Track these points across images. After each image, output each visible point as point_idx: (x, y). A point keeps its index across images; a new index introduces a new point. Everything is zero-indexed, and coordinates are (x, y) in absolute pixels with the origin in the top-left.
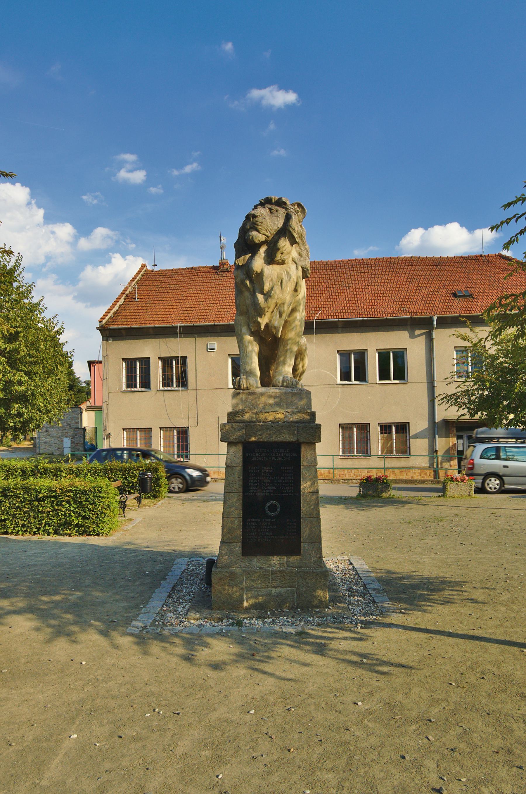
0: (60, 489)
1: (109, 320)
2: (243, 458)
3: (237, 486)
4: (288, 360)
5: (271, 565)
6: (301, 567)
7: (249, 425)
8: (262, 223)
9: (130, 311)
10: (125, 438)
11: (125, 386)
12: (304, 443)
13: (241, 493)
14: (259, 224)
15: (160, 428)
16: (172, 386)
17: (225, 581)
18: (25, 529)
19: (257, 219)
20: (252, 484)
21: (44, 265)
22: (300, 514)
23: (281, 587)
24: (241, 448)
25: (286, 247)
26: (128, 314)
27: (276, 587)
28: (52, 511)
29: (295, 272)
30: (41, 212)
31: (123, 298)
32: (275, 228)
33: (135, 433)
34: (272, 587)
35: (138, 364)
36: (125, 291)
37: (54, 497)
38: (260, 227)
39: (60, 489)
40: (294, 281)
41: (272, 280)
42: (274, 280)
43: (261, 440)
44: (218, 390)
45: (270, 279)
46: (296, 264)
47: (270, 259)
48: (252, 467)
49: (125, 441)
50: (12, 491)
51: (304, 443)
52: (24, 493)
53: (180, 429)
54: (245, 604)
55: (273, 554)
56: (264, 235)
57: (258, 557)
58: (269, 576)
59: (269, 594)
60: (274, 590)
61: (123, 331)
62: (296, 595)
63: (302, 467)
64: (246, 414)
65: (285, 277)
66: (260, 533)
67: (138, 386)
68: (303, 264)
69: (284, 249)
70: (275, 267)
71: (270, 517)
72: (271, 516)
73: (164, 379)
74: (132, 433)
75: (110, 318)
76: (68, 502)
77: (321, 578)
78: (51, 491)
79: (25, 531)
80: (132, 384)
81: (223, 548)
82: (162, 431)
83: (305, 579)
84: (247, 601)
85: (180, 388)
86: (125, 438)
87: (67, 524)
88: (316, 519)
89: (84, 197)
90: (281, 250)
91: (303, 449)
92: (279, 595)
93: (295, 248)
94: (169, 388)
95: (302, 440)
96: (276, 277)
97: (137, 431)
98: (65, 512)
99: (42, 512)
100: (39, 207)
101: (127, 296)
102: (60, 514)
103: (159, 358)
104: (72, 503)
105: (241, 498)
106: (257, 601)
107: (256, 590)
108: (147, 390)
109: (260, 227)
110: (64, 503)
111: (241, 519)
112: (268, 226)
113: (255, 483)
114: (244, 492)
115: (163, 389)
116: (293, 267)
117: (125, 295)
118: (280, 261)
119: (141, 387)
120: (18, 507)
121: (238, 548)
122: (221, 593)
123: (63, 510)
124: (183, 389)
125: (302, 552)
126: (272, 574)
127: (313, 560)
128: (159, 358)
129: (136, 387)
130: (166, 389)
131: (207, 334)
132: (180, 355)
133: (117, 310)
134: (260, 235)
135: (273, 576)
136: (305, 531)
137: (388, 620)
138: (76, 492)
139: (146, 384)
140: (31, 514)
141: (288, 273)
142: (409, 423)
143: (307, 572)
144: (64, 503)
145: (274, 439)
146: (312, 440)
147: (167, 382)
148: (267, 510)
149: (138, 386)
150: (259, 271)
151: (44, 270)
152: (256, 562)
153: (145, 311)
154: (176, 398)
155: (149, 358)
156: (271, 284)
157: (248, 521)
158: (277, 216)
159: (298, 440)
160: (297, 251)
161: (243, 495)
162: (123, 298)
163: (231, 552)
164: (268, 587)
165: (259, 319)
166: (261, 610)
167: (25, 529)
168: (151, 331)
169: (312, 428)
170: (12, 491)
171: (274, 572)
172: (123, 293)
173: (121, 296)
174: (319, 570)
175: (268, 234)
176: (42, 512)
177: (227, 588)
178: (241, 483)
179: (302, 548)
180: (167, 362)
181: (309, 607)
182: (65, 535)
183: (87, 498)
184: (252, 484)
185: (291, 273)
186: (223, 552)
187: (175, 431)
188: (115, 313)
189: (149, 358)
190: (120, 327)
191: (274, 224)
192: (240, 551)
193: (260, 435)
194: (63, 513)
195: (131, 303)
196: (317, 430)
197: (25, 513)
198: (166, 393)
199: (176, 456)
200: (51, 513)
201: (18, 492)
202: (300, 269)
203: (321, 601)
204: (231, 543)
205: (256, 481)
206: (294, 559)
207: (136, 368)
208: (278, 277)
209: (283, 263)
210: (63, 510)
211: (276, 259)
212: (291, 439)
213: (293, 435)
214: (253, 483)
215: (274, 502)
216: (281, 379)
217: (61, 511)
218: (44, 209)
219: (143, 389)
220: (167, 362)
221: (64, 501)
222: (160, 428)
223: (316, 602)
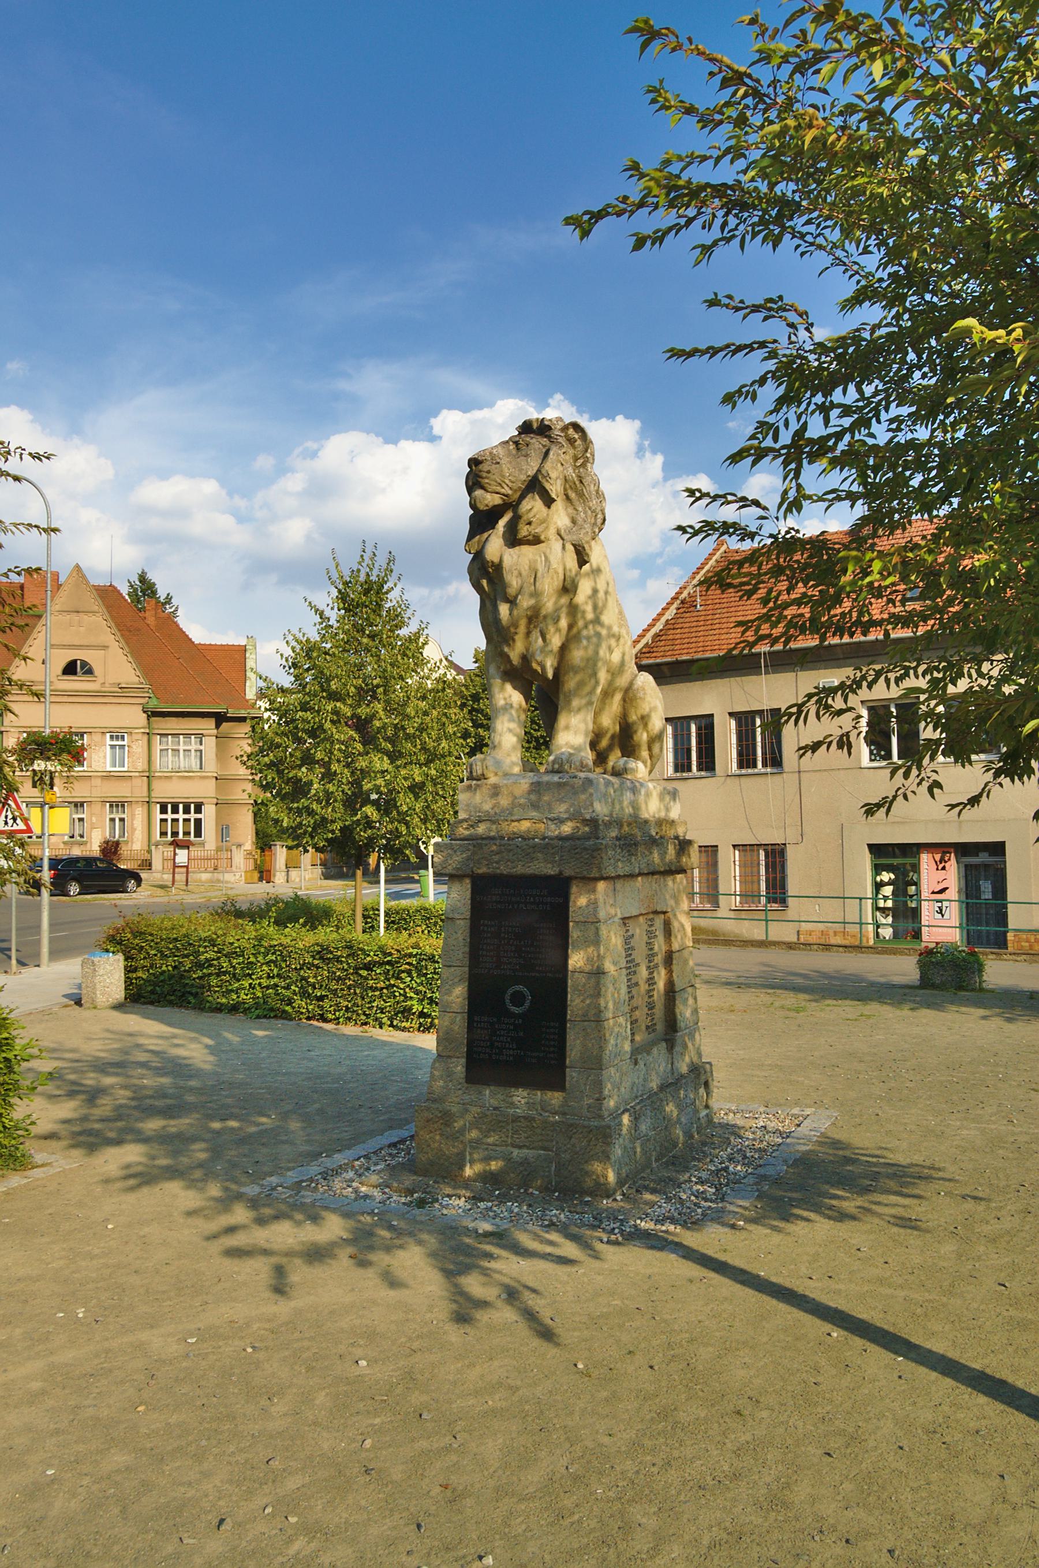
0: (398, 951)
1: (644, 650)
2: (472, 904)
3: (461, 956)
5: (512, 1105)
6: (564, 1114)
8: (488, 472)
9: (683, 631)
10: (737, 863)
11: (735, 765)
13: (467, 969)
14: (484, 475)
15: (734, 846)
16: (755, 766)
17: (436, 1126)
18: (350, 1015)
19: (480, 467)
21: (660, 554)
23: (528, 1148)
24: (469, 886)
25: (535, 510)
26: (677, 637)
27: (520, 1147)
28: (387, 988)
29: (560, 554)
30: (659, 459)
31: (675, 605)
32: (523, 477)
33: (755, 853)
34: (514, 1146)
35: (693, 728)
36: (679, 593)
37: (389, 963)
38: (487, 481)
39: (398, 951)
40: (557, 573)
41: (520, 574)
42: (524, 573)
43: (498, 871)
44: (842, 772)
45: (515, 573)
46: (563, 539)
47: (513, 540)
49: (737, 868)
50: (332, 953)
52: (348, 955)
53: (770, 847)
54: (468, 1172)
55: (517, 1085)
56: (497, 493)
57: (492, 1088)
58: (508, 1124)
59: (508, 1159)
60: (516, 1152)
61: (665, 669)
63: (571, 924)
65: (541, 568)
66: (496, 1044)
67: (694, 768)
68: (575, 537)
69: (531, 515)
70: (525, 549)
71: (513, 1015)
72: (513, 1013)
73: (740, 754)
74: (749, 853)
75: (647, 645)
76: (409, 973)
77: (597, 1139)
78: (386, 954)
79: (349, 1019)
80: (748, 761)
81: (437, 1065)
82: (737, 852)
83: (571, 1138)
84: (471, 1167)
85: (769, 770)
86: (737, 863)
87: (407, 1012)
88: (593, 1024)
89: (731, 425)
90: (525, 518)
91: (574, 889)
92: (525, 1162)
94: (750, 771)
95: (568, 872)
96: (527, 568)
97: (758, 851)
98: (404, 989)
99: (373, 989)
100: (654, 452)
101: (683, 602)
102: (397, 994)
103: (731, 714)
104: (415, 975)
106: (488, 1168)
108: (709, 774)
109: (487, 481)
110: (403, 975)
111: (466, 1015)
112: (503, 476)
114: (471, 967)
115: (738, 772)
116: (556, 545)
117: (679, 602)
118: (530, 538)
119: (699, 769)
120: (340, 978)
121: (459, 1068)
122: (429, 1146)
123: (402, 986)
124: (775, 771)
125: (567, 1085)
127: (587, 1101)
128: (731, 714)
129: (690, 770)
130: (744, 771)
131: (818, 664)
132: (766, 706)
133: (661, 631)
134: (488, 496)
136: (575, 1045)
137: (691, 1239)
138: (422, 957)
139: (708, 762)
140: (358, 991)
141: (546, 558)
143: (572, 1125)
144: (403, 975)
145: (520, 869)
146: (585, 873)
147: (746, 759)
148: (507, 1001)
149: (694, 768)
150: (496, 560)
151: (659, 561)
152: (490, 1096)
153: (709, 627)
154: (765, 789)
155: (712, 715)
156: (520, 582)
158: (526, 456)
159: (561, 873)
160: (568, 515)
161: (470, 970)
162: (675, 605)
163: (449, 1075)
165: (506, 649)
166: (492, 1187)
167: (350, 1014)
168: (665, 669)
169: (585, 849)
170: (332, 953)
171: (516, 1119)
172: (674, 599)
173: (670, 604)
174: (595, 1123)
175: (507, 490)
176: (373, 989)
177: (438, 1137)
178: (467, 949)
179: (567, 1079)
180: (744, 720)
181: (576, 1192)
182: (404, 1029)
183: (435, 968)
185: (552, 558)
186: (436, 1073)
187: (762, 853)
188: (657, 635)
189: (712, 715)
190: (658, 661)
191: (521, 470)
192: (463, 1075)
193: (497, 863)
194: (402, 992)
195: (688, 615)
196: (595, 854)
197: (349, 988)
198: (743, 780)
199: (763, 900)
200: (385, 991)
201: (339, 953)
202: (570, 548)
203: (598, 1184)
204: (449, 1057)
206: (555, 1098)
207: (689, 735)
208: (530, 568)
209: (536, 541)
210: (402, 986)
211: (519, 536)
212: (550, 870)
213: (553, 862)
215: (515, 1010)
217: (398, 987)
218: (662, 453)
219: (703, 773)
220: (744, 720)
221: (403, 972)
222: (734, 846)
223: (589, 1183)
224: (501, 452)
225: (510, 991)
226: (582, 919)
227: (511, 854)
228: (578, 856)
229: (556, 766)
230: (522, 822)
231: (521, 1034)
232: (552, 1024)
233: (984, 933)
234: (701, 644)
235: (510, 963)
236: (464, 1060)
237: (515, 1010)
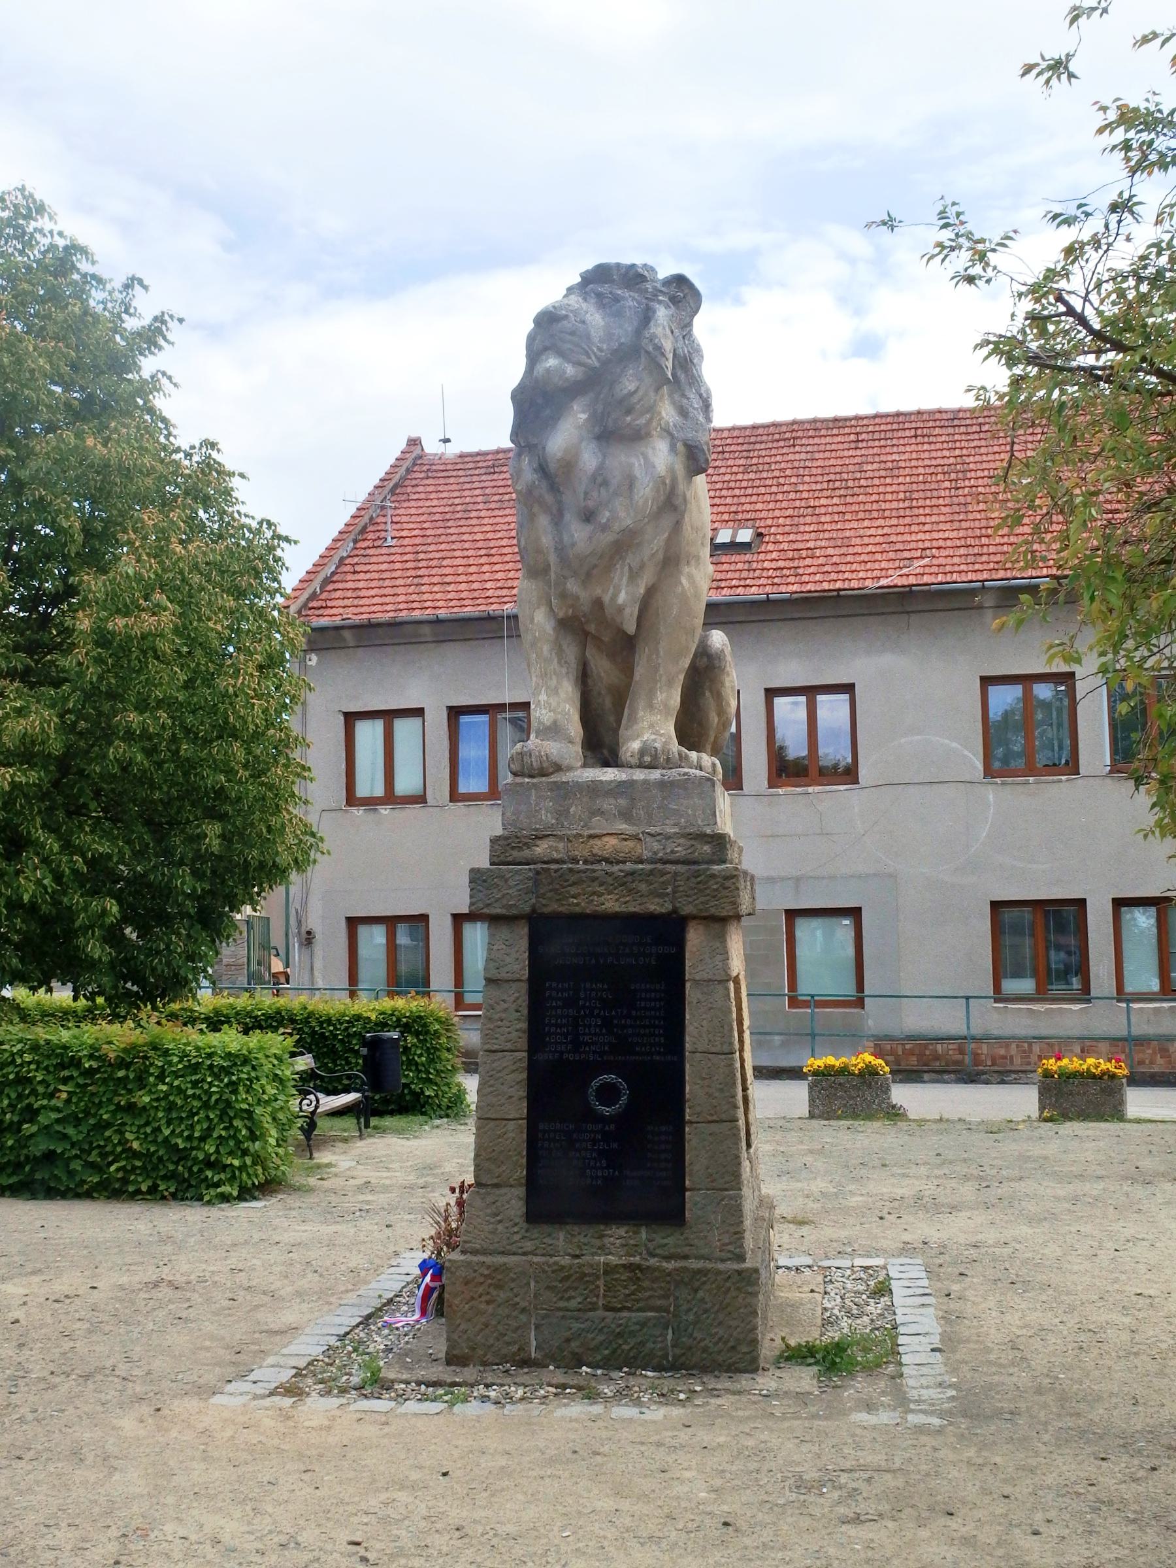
4: (660, 697)
7: (545, 874)
9: (368, 576)
12: (694, 917)
13: (525, 1054)
17: (481, 1290)
20: (553, 1029)
22: (683, 1111)
43: (577, 909)
48: (554, 984)
51: (694, 917)
57: (568, 1227)
58: (598, 1278)
62: (670, 1331)
63: (688, 985)
64: (539, 842)
71: (602, 1119)
83: (696, 1291)
93: (670, 395)
95: (687, 910)
105: (525, 1064)
107: (563, 1317)
113: (561, 1026)
121: (514, 1202)
126: (606, 1273)
133: (333, 574)
135: (608, 1278)
142: (995, 905)
157: (541, 1126)
164: (594, 1309)
169: (713, 876)
178: (524, 1025)
184: (553, 1029)
196: (728, 883)
202: (680, 446)
205: (565, 1021)
214: (556, 1025)
215: (606, 1110)
216: (635, 745)
224: (575, 301)
225: (595, 1084)
226: (706, 977)
227: (596, 883)
228: (701, 886)
229: (647, 759)
230: (606, 839)
231: (615, 1145)
232: (664, 1129)
233: (755, 1037)
234: (402, 598)
235: (593, 1043)
236: (521, 1191)
237: (606, 1110)
